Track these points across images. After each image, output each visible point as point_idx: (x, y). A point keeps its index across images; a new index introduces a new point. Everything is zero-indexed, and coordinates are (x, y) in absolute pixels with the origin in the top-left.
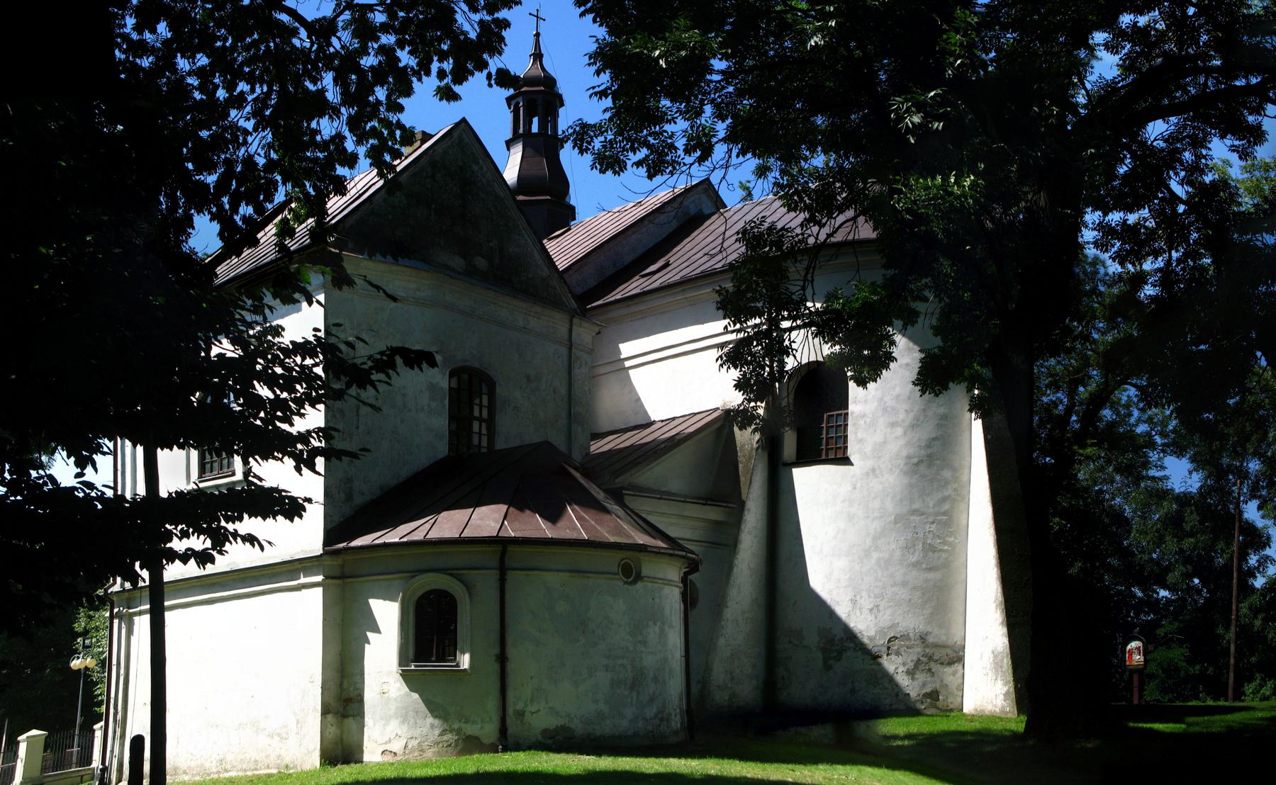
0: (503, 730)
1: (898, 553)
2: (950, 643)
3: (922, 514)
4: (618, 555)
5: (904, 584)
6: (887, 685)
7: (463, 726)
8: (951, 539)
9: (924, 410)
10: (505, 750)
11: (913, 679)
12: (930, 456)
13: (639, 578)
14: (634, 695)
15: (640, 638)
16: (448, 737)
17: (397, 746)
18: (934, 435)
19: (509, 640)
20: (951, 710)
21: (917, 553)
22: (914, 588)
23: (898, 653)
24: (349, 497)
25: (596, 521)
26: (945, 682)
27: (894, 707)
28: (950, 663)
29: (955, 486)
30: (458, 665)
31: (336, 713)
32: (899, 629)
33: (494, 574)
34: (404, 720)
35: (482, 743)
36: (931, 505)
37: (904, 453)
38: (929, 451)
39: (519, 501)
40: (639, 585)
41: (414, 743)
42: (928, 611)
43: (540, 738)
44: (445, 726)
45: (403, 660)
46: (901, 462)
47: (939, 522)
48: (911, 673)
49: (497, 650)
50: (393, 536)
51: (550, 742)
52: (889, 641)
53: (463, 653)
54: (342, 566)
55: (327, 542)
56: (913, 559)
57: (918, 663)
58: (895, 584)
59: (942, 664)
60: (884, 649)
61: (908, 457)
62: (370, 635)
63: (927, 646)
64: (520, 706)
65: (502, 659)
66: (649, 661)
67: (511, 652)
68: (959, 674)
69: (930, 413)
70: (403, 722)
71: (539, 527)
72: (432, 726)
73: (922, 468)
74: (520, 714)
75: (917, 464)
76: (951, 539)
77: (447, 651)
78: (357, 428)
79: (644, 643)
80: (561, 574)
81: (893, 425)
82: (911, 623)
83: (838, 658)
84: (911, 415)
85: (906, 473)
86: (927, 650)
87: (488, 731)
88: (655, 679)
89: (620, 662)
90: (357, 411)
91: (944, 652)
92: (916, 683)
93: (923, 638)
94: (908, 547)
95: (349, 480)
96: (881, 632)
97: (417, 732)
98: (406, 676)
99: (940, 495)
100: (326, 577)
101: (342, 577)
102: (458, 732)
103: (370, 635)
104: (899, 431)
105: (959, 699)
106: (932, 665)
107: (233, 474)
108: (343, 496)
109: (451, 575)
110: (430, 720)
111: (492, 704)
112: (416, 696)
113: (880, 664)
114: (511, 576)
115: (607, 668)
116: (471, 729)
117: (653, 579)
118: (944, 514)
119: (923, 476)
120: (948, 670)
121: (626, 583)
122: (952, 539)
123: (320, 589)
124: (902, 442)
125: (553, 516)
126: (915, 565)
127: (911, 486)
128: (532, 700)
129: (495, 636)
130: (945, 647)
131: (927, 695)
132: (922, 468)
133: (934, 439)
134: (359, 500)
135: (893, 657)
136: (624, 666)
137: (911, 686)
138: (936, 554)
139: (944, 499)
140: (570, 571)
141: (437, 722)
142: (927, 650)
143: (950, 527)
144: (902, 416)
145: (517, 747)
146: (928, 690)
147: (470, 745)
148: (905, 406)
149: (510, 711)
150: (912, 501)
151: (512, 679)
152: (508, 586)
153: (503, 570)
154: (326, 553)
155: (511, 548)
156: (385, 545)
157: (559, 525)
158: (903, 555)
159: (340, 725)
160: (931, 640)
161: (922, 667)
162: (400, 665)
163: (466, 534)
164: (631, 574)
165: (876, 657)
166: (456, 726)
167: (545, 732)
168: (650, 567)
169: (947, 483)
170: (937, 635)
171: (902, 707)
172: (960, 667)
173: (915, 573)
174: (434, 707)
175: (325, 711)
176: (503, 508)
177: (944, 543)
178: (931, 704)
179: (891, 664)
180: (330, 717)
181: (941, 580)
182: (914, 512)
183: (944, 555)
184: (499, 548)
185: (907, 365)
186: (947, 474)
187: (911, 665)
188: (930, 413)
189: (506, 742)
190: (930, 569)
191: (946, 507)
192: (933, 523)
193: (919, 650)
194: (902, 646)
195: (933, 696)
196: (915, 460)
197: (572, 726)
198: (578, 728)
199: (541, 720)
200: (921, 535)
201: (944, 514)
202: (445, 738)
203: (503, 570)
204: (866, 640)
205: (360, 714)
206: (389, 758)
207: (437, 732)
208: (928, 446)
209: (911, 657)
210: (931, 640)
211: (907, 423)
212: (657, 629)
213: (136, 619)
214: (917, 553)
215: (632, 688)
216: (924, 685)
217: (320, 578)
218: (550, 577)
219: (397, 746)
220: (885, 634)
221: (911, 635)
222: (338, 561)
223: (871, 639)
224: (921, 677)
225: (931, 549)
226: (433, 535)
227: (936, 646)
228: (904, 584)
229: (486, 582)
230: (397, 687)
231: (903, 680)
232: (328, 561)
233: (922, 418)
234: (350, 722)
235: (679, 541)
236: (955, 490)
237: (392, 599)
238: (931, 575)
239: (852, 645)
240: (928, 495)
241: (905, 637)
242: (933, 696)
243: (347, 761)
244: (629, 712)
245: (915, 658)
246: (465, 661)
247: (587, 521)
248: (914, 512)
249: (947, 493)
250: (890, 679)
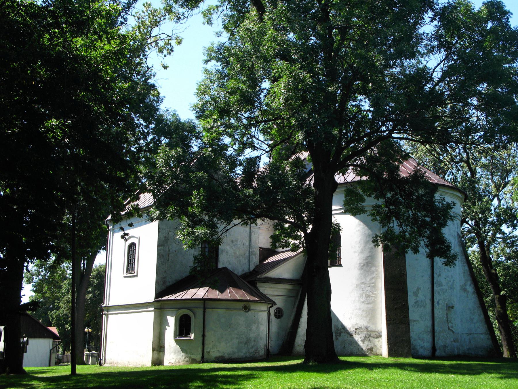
0: (203, 357)
1: (357, 298)
2: (376, 330)
3: (365, 284)
4: (243, 303)
5: (360, 309)
6: (355, 345)
7: (191, 356)
8: (375, 293)
9: (365, 246)
10: (203, 363)
11: (364, 343)
12: (367, 263)
13: (249, 310)
14: (246, 346)
15: (249, 329)
16: (187, 359)
17: (173, 361)
18: (368, 255)
19: (206, 330)
20: (377, 355)
21: (364, 298)
22: (363, 310)
23: (358, 334)
24: (164, 283)
25: (236, 293)
26: (375, 344)
27: (358, 353)
28: (377, 337)
29: (376, 273)
30: (190, 338)
31: (157, 351)
32: (359, 325)
33: (202, 310)
34: (175, 353)
35: (197, 361)
36: (368, 280)
37: (358, 262)
38: (367, 261)
39: (213, 286)
40: (250, 312)
41: (177, 360)
42: (368, 319)
43: (214, 359)
44: (186, 355)
45: (175, 336)
46: (358, 265)
47: (371, 287)
48: (363, 341)
49: (202, 333)
50: (173, 297)
51: (217, 360)
52: (355, 330)
53: (192, 333)
54: (161, 305)
55: (156, 298)
56: (362, 300)
57: (365, 337)
58: (357, 309)
59: (374, 338)
60: (354, 332)
61: (360, 264)
62: (167, 327)
63: (368, 332)
64: (208, 350)
65: (204, 336)
66: (252, 336)
67: (207, 334)
68: (380, 342)
69: (367, 247)
70: (175, 354)
71: (216, 294)
72: (183, 356)
73: (365, 267)
74: (208, 352)
75: (363, 266)
76: (375, 293)
77: (188, 333)
78: (168, 261)
79: (251, 330)
80: (223, 310)
81: (355, 252)
82: (362, 323)
83: (340, 336)
84: (360, 248)
85: (359, 269)
86: (368, 333)
87: (199, 357)
88: (254, 341)
89: (241, 336)
90: (169, 256)
91: (374, 333)
92: (365, 345)
93: (367, 328)
94: (361, 296)
95: (164, 278)
96: (353, 326)
97: (178, 357)
98: (176, 340)
99: (371, 277)
100: (155, 309)
101: (161, 309)
102: (190, 357)
103: (167, 327)
104: (357, 254)
105: (381, 351)
106: (370, 338)
107: (134, 273)
108: (162, 283)
109: (189, 310)
110: (182, 354)
111: (200, 350)
112: (178, 346)
113: (353, 338)
114: (207, 310)
115: (237, 338)
116: (193, 357)
117: (254, 310)
118: (373, 283)
119: (365, 270)
120: (376, 340)
121: (245, 312)
122: (376, 292)
123: (153, 312)
124: (358, 258)
125: (222, 291)
126: (363, 302)
127: (361, 274)
128: (212, 348)
129: (202, 329)
130: (375, 331)
131: (369, 349)
132: (365, 267)
133: (368, 257)
134: (168, 284)
135: (357, 335)
136: (243, 337)
137: (364, 346)
138: (370, 298)
139: (373, 278)
140: (226, 309)
141: (184, 354)
142: (368, 333)
143: (375, 288)
144: (357, 249)
145: (207, 362)
146: (369, 347)
147: (193, 361)
148: (358, 245)
149: (205, 351)
150: (362, 279)
151: (206, 342)
152: (207, 314)
153: (205, 309)
154: (155, 301)
155: (206, 302)
156: (171, 300)
157: (223, 294)
158: (359, 299)
159: (159, 354)
160: (369, 329)
161: (367, 339)
162: (174, 337)
163: (195, 297)
164: (246, 309)
165: (351, 335)
166: (189, 356)
167: (216, 358)
168: (253, 306)
169: (373, 272)
170: (372, 327)
171: (360, 353)
172: (381, 339)
173: (363, 305)
174: (183, 350)
175: (154, 350)
176: (208, 288)
177: (373, 294)
178: (370, 352)
179: (357, 338)
180: (155, 352)
181: (372, 307)
182: (362, 283)
183: (373, 298)
184: (203, 302)
185: (359, 230)
186: (373, 269)
187: (363, 338)
188: (367, 247)
189: (203, 361)
190: (368, 304)
191: (373, 281)
192: (369, 287)
193: (365, 333)
194: (359, 331)
195: (371, 349)
196: (362, 265)
197: (225, 355)
198: (226, 356)
199: (215, 354)
200: (365, 291)
201: (373, 283)
202: (186, 359)
203: (205, 309)
204: (348, 329)
205: (163, 351)
206: (170, 365)
207: (184, 357)
208: (367, 259)
209: (363, 335)
210: (369, 329)
211: (359, 251)
212: (256, 326)
213: (109, 316)
214: (364, 298)
215: (245, 344)
216: (368, 345)
217: (153, 309)
218: (219, 310)
219: (173, 361)
220: (354, 327)
221: (363, 327)
222: (159, 304)
223: (349, 328)
224: (367, 343)
225: (368, 296)
226: (184, 298)
227: (372, 331)
228: (360, 309)
229: (199, 312)
230: (174, 344)
231: (361, 343)
232: (156, 304)
233: (364, 249)
234: (161, 353)
235: (257, 299)
236: (376, 274)
237: (173, 317)
238: (369, 306)
239: (344, 331)
240: (367, 277)
241: (360, 328)
242: (371, 349)
243: (159, 365)
244: (244, 351)
245: (364, 336)
246: (192, 336)
247: (233, 292)
248: (362, 283)
249: (373, 276)
250: (356, 343)
